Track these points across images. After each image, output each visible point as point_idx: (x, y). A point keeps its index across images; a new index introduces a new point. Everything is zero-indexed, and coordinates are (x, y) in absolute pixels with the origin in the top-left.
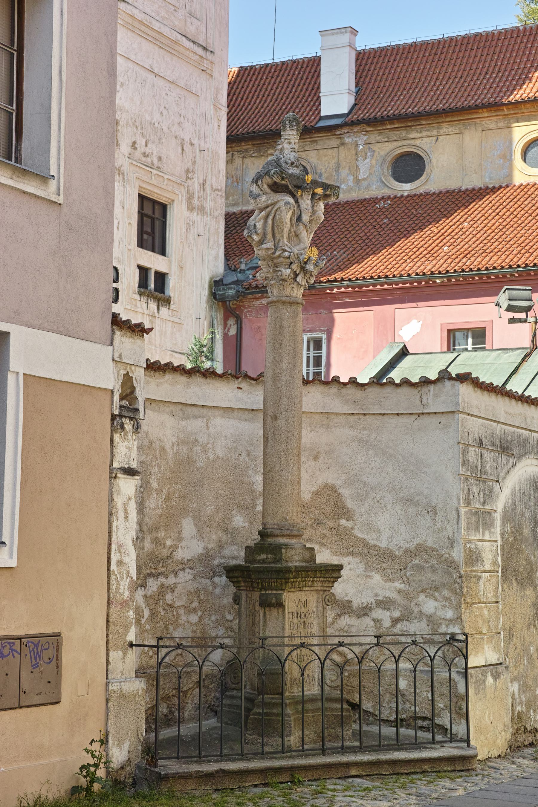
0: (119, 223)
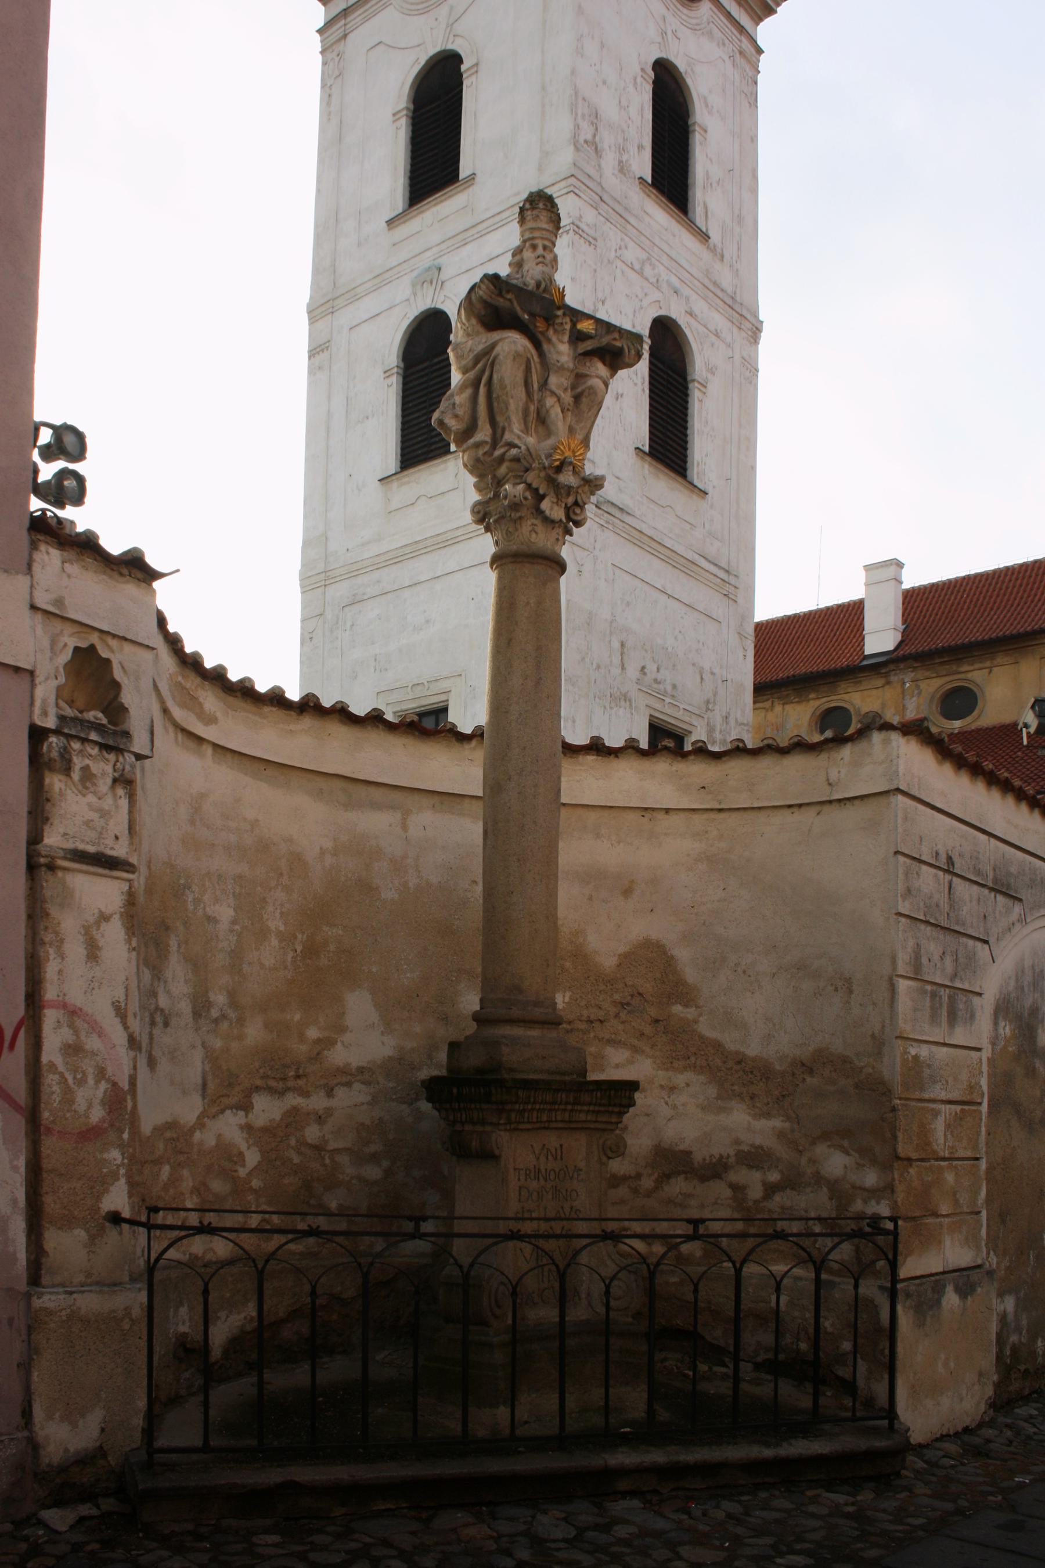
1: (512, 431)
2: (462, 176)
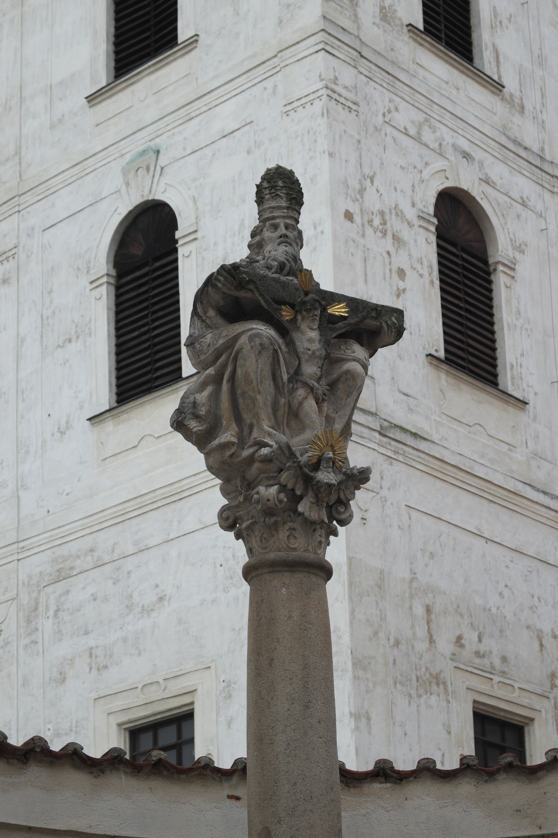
0: (443, 755)
1: (262, 429)
2: (181, 37)
